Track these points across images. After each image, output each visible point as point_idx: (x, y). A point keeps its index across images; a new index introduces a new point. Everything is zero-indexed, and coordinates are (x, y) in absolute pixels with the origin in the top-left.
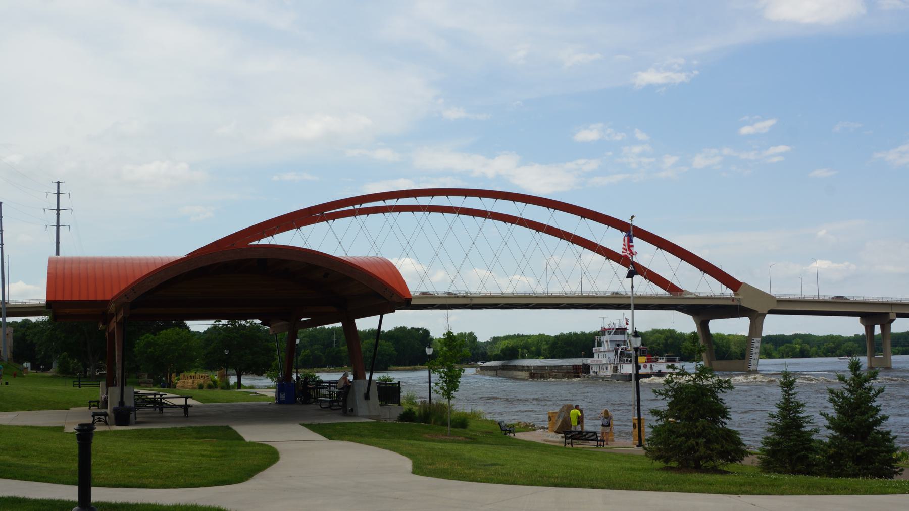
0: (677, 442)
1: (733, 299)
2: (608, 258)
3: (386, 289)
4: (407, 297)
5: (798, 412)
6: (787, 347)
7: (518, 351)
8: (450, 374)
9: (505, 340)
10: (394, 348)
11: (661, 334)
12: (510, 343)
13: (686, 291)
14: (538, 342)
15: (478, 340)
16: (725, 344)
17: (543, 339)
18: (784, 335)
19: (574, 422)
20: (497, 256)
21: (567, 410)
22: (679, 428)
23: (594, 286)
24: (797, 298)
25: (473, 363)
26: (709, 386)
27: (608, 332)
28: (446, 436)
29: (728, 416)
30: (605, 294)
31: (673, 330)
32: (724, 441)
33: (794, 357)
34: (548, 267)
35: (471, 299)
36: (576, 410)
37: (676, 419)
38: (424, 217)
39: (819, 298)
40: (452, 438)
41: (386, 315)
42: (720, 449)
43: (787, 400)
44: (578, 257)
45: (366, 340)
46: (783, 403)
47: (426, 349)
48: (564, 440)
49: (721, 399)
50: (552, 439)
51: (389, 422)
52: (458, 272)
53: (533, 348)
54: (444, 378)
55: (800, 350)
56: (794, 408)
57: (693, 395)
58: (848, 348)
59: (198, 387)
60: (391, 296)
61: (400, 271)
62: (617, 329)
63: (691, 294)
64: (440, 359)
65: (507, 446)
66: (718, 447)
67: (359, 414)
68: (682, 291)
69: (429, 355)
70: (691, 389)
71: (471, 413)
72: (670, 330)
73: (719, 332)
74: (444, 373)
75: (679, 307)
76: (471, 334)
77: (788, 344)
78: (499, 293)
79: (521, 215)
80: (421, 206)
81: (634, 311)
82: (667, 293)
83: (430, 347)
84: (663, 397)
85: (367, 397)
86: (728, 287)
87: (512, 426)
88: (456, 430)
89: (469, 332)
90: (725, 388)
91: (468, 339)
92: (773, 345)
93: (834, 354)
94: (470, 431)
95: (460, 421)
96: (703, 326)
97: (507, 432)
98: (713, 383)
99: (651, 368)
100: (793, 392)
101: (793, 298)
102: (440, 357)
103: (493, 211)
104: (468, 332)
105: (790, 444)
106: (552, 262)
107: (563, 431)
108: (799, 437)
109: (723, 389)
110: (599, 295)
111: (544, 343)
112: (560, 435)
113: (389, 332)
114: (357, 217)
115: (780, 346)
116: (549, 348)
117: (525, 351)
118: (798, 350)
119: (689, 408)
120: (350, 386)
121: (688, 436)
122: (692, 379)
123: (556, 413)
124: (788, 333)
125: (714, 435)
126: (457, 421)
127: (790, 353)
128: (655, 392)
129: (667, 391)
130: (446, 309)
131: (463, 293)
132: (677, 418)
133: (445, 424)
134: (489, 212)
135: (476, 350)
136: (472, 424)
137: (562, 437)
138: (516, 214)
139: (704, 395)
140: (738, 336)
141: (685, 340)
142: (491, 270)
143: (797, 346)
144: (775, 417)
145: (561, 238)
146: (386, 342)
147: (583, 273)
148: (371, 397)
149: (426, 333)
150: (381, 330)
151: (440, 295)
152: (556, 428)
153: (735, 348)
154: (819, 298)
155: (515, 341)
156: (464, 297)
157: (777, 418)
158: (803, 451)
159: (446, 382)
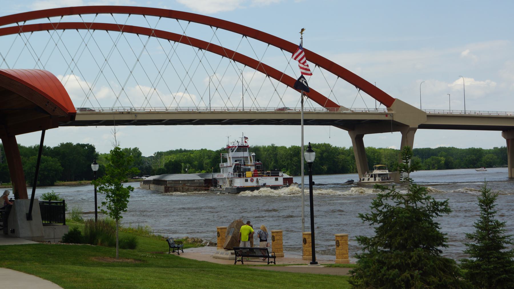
0: (389, 275)
1: (387, 115)
2: (269, 75)
3: (48, 102)
4: (71, 111)
5: (498, 232)
6: (433, 159)
7: (181, 166)
8: (118, 192)
9: (167, 155)
10: (60, 164)
11: (317, 148)
12: (173, 158)
13: (342, 107)
14: (200, 157)
15: (142, 155)
16: (376, 157)
17: (205, 154)
18: (430, 149)
19: (245, 237)
20: (161, 73)
21: (236, 226)
22: (391, 258)
23: (255, 102)
24: (446, 113)
25: (137, 177)
26: (423, 209)
27: (231, 149)
28: (114, 258)
29: (444, 243)
30: (266, 110)
31: (328, 144)
32: (442, 273)
33: (439, 168)
34: (211, 84)
35: (136, 116)
36: (248, 226)
37: (385, 248)
38: (89, 35)
39: (465, 113)
40: (121, 261)
41: (49, 130)
42: (439, 283)
43: (486, 220)
44: (239, 74)
45: (32, 156)
46: (481, 223)
47: (92, 165)
48: (234, 256)
49: (437, 224)
50: (222, 256)
51: (52, 243)
52: (123, 89)
53: (196, 163)
54: (112, 197)
55: (445, 162)
56: (494, 228)
57: (407, 220)
58: (488, 160)
59: (388, 115)
60: (54, 110)
61: (66, 88)
62: (239, 147)
63: (347, 109)
64: (107, 176)
65: (179, 269)
66: (436, 280)
67: (21, 236)
68: (339, 106)
69: (95, 172)
70: (405, 213)
71: (138, 229)
72: (326, 144)
73: (370, 146)
74: (111, 192)
75: (335, 122)
76: (136, 150)
77: (434, 157)
78: (163, 110)
79: (184, 33)
80: (86, 23)
81: (304, 126)
82: (324, 109)
83: (95, 164)
84: (371, 222)
85: (29, 217)
86: (381, 102)
87: (180, 242)
88: (125, 251)
89: (134, 147)
90: (441, 211)
91: (132, 154)
92: (420, 158)
93: (475, 165)
94: (140, 251)
95: (128, 241)
96: (358, 141)
97: (175, 249)
98: (427, 206)
99: (257, 182)
100: (492, 211)
101: (441, 113)
102: (107, 175)
103: (156, 29)
104: (132, 147)
105: (490, 267)
106: (214, 79)
107: (234, 248)
108: (499, 258)
109: (438, 213)
110: (260, 111)
111: (206, 157)
112: (230, 252)
113: (55, 148)
114: (21, 34)
115: (426, 158)
116: (211, 162)
117: (188, 165)
118: (443, 162)
119: (401, 235)
120: (11, 206)
121: (401, 268)
122: (403, 201)
123: (226, 228)
124: (434, 147)
125: (431, 266)
126: (126, 241)
127: (436, 165)
128: (362, 216)
129: (375, 215)
130: (113, 125)
131: (128, 109)
132: (386, 246)
133: (112, 244)
134: (153, 29)
135: (141, 165)
136: (140, 241)
137: (232, 254)
138: (180, 32)
139: (419, 220)
140: (388, 150)
141: (339, 153)
142: (155, 86)
143: (442, 158)
144: (473, 238)
145: (224, 55)
146: (52, 158)
147: (244, 90)
148: (33, 217)
149: (91, 148)
150: (44, 144)
151: (105, 111)
152: (225, 245)
153: (386, 161)
154: (465, 113)
155: (178, 155)
156: (128, 113)
157: (475, 239)
158: (503, 274)
159: (113, 201)
